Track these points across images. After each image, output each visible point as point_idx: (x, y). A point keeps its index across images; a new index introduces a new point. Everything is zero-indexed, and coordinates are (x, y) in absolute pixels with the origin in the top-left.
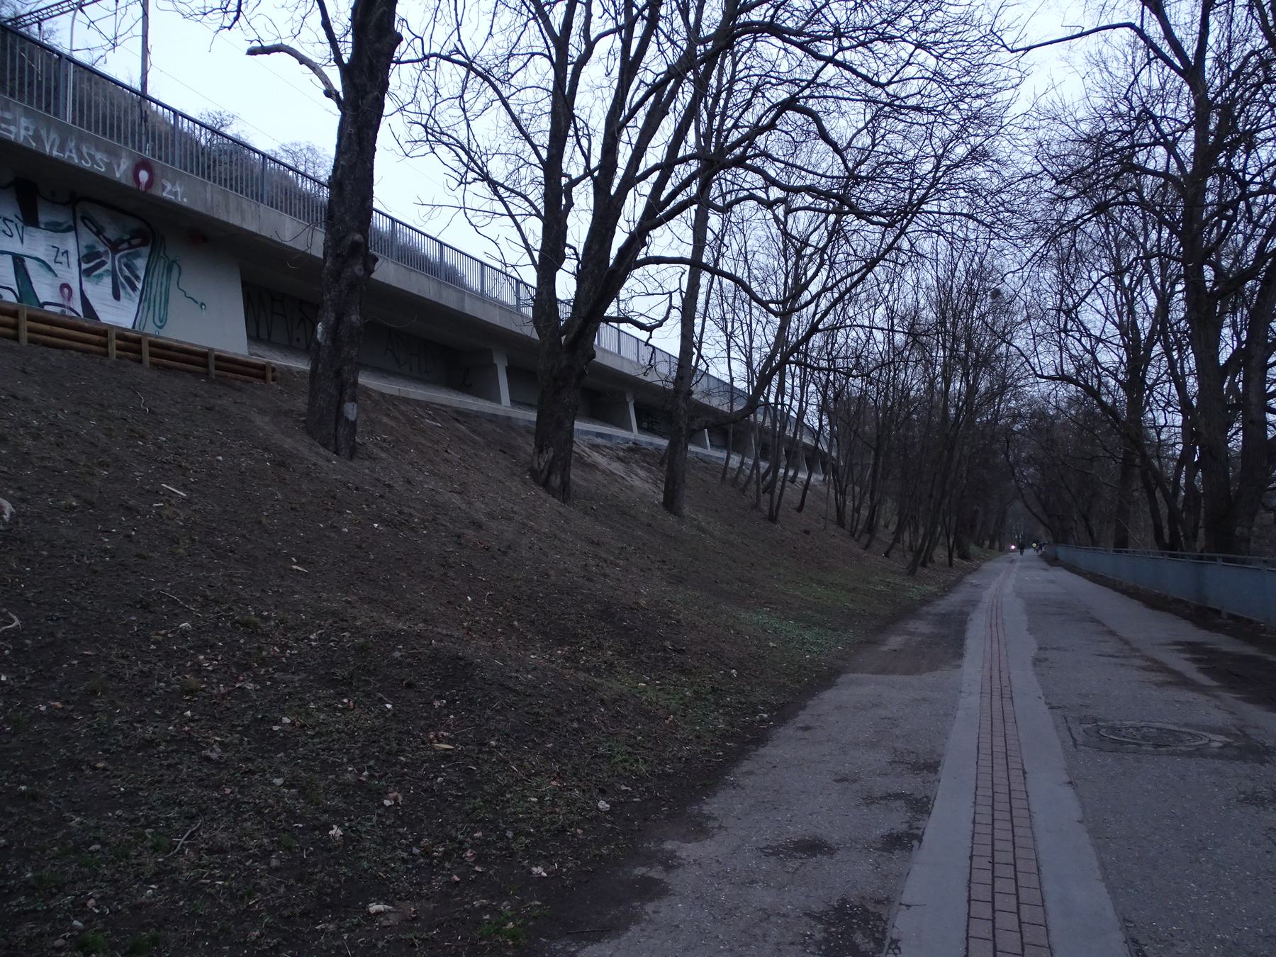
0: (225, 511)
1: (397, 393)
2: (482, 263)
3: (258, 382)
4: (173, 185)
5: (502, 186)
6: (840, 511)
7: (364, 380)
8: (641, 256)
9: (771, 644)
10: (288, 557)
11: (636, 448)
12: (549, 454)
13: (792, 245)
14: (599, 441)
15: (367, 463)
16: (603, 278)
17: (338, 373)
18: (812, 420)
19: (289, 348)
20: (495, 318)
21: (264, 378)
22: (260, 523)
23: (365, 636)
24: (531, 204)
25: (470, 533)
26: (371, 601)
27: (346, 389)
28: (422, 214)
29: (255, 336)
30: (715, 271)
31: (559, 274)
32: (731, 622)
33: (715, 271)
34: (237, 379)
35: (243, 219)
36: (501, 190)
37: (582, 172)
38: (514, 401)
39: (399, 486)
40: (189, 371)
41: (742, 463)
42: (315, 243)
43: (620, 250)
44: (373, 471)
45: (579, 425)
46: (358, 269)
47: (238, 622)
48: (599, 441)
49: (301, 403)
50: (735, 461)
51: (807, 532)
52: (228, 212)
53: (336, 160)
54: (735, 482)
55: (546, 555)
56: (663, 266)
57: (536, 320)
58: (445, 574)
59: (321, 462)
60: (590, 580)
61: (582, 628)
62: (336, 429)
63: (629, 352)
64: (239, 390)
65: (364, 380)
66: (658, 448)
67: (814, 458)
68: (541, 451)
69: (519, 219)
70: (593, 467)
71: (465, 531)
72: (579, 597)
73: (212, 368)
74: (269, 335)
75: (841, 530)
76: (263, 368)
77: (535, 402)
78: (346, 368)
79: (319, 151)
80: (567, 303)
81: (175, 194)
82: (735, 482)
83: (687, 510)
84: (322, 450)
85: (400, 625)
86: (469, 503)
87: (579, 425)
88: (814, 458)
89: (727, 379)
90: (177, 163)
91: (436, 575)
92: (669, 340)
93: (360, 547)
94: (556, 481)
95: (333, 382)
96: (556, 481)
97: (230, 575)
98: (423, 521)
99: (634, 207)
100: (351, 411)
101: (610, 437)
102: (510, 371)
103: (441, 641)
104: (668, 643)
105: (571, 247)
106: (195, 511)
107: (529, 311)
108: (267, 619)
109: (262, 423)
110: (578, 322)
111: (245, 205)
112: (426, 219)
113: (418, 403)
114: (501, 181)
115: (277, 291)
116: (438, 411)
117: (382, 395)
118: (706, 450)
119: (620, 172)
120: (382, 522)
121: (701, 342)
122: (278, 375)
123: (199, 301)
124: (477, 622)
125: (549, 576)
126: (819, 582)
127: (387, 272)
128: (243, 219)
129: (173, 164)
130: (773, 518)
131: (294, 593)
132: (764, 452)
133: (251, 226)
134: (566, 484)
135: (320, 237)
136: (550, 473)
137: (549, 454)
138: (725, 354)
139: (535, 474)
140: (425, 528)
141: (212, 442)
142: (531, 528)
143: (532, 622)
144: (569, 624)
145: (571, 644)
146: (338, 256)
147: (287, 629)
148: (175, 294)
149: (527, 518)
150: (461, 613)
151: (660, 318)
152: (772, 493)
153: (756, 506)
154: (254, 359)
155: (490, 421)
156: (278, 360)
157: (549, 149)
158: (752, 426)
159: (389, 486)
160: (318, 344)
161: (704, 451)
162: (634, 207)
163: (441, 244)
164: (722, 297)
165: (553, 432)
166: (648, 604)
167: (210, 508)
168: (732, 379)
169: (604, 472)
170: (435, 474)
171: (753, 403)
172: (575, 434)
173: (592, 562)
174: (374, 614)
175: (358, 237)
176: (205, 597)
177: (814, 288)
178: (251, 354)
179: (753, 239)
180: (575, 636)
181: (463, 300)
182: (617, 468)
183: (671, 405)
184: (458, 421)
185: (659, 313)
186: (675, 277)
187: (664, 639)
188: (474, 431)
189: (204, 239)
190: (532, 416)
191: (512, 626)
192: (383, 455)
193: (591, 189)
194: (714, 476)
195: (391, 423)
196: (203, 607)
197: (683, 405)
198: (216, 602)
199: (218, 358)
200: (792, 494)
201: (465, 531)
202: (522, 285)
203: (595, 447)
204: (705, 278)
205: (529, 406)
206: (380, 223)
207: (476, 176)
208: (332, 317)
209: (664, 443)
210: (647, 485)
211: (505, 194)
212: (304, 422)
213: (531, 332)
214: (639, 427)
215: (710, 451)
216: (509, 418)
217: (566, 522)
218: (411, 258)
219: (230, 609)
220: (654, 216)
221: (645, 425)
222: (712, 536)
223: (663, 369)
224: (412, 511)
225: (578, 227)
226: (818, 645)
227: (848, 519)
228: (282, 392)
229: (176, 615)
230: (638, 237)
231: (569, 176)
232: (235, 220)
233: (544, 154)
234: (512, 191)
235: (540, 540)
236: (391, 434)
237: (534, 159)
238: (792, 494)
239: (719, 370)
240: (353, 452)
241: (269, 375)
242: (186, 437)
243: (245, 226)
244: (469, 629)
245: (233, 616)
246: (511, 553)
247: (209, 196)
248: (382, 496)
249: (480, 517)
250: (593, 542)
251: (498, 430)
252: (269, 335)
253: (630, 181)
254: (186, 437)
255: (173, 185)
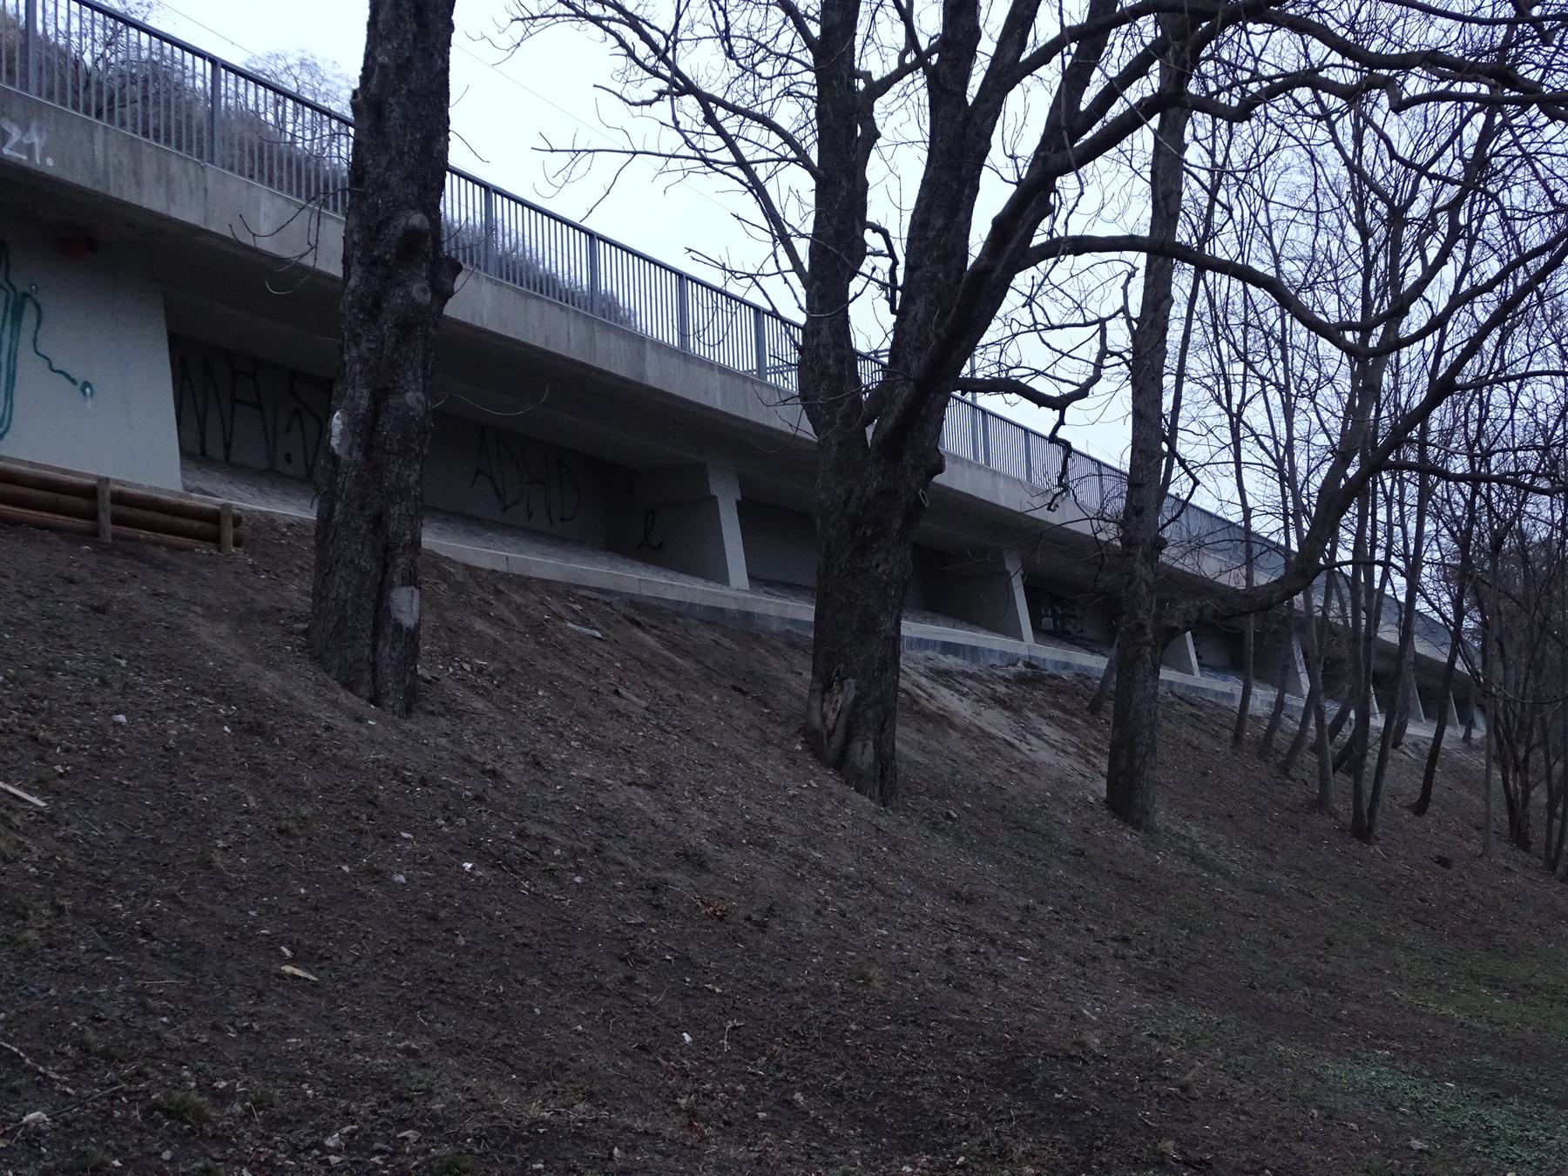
0: (130, 840)
1: (502, 567)
2: (681, 276)
3: (203, 549)
4: (25, 129)
5: (721, 103)
6: (1516, 808)
7: (434, 540)
8: (1039, 239)
9: (1417, 1144)
10: (271, 945)
11: (1033, 677)
12: (845, 695)
13: (1378, 208)
14: (950, 661)
15: (443, 723)
16: (953, 295)
17: (378, 522)
18: (1435, 602)
19: (270, 475)
20: (714, 397)
21: (216, 539)
22: (209, 865)
23: (454, 1139)
24: (787, 138)
25: (679, 880)
26: (460, 1048)
27: (393, 556)
28: (551, 172)
29: (195, 454)
30: (1204, 264)
31: (855, 285)
32: (1306, 1086)
33: (1204, 264)
34: (156, 544)
35: (171, 198)
36: (720, 113)
37: (894, 65)
38: (757, 579)
39: (515, 772)
40: (53, 529)
41: (1280, 704)
42: (325, 246)
43: (999, 223)
44: (458, 742)
45: (911, 628)
46: (419, 291)
47: (157, 1106)
48: (950, 661)
49: (297, 594)
50: (1262, 698)
51: (1444, 862)
52: (139, 184)
53: (369, 56)
54: (1264, 748)
55: (854, 928)
56: (1087, 259)
57: (806, 395)
58: (630, 979)
59: (341, 722)
60: (963, 988)
61: (957, 1108)
62: (374, 648)
63: (1007, 457)
64: (162, 566)
65: (434, 540)
66: (1083, 675)
67: (1442, 693)
68: (827, 688)
69: (761, 172)
70: (942, 720)
71: (668, 875)
72: (945, 1031)
73: (105, 519)
74: (227, 447)
75: (1520, 855)
76: (214, 517)
77: (812, 583)
78: (395, 510)
79: (326, 69)
80: (873, 356)
81: (30, 149)
82: (1264, 748)
83: (1161, 816)
84: (343, 696)
85: (534, 1110)
86: (673, 809)
87: (911, 628)
88: (1442, 693)
89: (1235, 515)
90: (33, 87)
91: (609, 981)
92: (1104, 430)
93: (434, 918)
94: (863, 754)
95: (367, 545)
96: (863, 754)
97: (141, 992)
98: (574, 853)
99: (1026, 114)
100: (406, 605)
101: (973, 652)
102: (743, 508)
103: (634, 1148)
104: (1169, 1145)
105: (877, 229)
106: (63, 840)
107: (791, 383)
108: (222, 1098)
109: (213, 636)
110: (905, 391)
111: (175, 167)
112: (559, 181)
113: (548, 585)
114: (719, 95)
115: (248, 356)
116: (593, 602)
117: (471, 570)
118: (1191, 676)
119: (987, 46)
120: (482, 856)
121: (1174, 428)
122: (245, 530)
123: (79, 374)
124: (709, 1096)
125: (868, 981)
126: (1494, 983)
127: (475, 302)
128: (171, 198)
129: (25, 86)
130: (1362, 830)
131: (287, 1032)
132: (1328, 677)
133: (188, 213)
134: (886, 762)
135: (334, 232)
136: (848, 740)
137: (845, 695)
138: (1227, 455)
139: (814, 740)
140: (578, 870)
141: (104, 683)
142: (817, 865)
143: (838, 1094)
144: (926, 1099)
145: (933, 1149)
146: (374, 263)
147: (274, 1123)
148: (28, 364)
149: (806, 841)
150: (670, 1073)
151: (1082, 380)
152: (1356, 770)
153: (1320, 804)
154: (196, 500)
155: (709, 623)
156: (247, 501)
157: (824, 22)
158: (1302, 623)
159: (494, 774)
160: (335, 458)
161: (1188, 680)
162: (1026, 114)
163: (591, 235)
164: (1218, 326)
165: (852, 647)
166: (1105, 1044)
167: (98, 831)
168: (1247, 511)
169: (966, 732)
170: (593, 746)
171: (1306, 566)
172: (904, 645)
173: (961, 945)
174: (472, 1082)
175: (417, 219)
176: (84, 1047)
177: (1439, 293)
178: (186, 488)
179: (1287, 187)
180: (941, 1127)
181: (641, 357)
182: (995, 721)
183: (1113, 578)
184: (638, 624)
185: (1077, 372)
186: (1109, 286)
187: (1160, 1135)
188: (673, 647)
189: (91, 244)
190: (804, 611)
191: (790, 1104)
192: (479, 705)
193: (924, 95)
194: (1216, 736)
195: (494, 633)
196: (78, 1070)
197: (1142, 570)
198: (108, 1057)
199: (119, 498)
200: (1403, 777)
201: (668, 875)
202: (769, 324)
203: (943, 676)
204: (1182, 280)
205: (792, 588)
206: (459, 205)
207: (664, 85)
208: (363, 398)
209: (1096, 663)
210: (1065, 762)
211: (731, 125)
212: (305, 632)
213: (794, 422)
214: (1037, 629)
215: (1198, 679)
216: (748, 616)
217: (894, 848)
218: (521, 275)
219: (140, 1074)
220: (1069, 143)
221: (1048, 622)
222: (1226, 874)
223: (1089, 494)
224: (548, 831)
225: (895, 181)
226: (1533, 1144)
227: (1538, 834)
228: (255, 570)
229: (14, 1091)
230: (1033, 196)
231: (867, 76)
232: (153, 200)
233: (815, 30)
234: (747, 113)
235: (839, 892)
236: (493, 657)
237: (788, 39)
238: (1403, 777)
239: (1214, 495)
240: (412, 702)
241: (229, 534)
242: (48, 672)
243: (177, 213)
244: (692, 1114)
245: (147, 1092)
246: (774, 924)
247: (99, 149)
248: (479, 799)
249: (698, 840)
250: (958, 897)
251: (726, 642)
252: (227, 447)
253: (1007, 72)
254: (48, 672)
255: (25, 129)
